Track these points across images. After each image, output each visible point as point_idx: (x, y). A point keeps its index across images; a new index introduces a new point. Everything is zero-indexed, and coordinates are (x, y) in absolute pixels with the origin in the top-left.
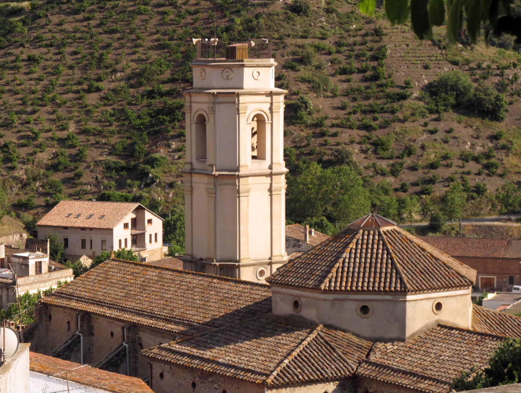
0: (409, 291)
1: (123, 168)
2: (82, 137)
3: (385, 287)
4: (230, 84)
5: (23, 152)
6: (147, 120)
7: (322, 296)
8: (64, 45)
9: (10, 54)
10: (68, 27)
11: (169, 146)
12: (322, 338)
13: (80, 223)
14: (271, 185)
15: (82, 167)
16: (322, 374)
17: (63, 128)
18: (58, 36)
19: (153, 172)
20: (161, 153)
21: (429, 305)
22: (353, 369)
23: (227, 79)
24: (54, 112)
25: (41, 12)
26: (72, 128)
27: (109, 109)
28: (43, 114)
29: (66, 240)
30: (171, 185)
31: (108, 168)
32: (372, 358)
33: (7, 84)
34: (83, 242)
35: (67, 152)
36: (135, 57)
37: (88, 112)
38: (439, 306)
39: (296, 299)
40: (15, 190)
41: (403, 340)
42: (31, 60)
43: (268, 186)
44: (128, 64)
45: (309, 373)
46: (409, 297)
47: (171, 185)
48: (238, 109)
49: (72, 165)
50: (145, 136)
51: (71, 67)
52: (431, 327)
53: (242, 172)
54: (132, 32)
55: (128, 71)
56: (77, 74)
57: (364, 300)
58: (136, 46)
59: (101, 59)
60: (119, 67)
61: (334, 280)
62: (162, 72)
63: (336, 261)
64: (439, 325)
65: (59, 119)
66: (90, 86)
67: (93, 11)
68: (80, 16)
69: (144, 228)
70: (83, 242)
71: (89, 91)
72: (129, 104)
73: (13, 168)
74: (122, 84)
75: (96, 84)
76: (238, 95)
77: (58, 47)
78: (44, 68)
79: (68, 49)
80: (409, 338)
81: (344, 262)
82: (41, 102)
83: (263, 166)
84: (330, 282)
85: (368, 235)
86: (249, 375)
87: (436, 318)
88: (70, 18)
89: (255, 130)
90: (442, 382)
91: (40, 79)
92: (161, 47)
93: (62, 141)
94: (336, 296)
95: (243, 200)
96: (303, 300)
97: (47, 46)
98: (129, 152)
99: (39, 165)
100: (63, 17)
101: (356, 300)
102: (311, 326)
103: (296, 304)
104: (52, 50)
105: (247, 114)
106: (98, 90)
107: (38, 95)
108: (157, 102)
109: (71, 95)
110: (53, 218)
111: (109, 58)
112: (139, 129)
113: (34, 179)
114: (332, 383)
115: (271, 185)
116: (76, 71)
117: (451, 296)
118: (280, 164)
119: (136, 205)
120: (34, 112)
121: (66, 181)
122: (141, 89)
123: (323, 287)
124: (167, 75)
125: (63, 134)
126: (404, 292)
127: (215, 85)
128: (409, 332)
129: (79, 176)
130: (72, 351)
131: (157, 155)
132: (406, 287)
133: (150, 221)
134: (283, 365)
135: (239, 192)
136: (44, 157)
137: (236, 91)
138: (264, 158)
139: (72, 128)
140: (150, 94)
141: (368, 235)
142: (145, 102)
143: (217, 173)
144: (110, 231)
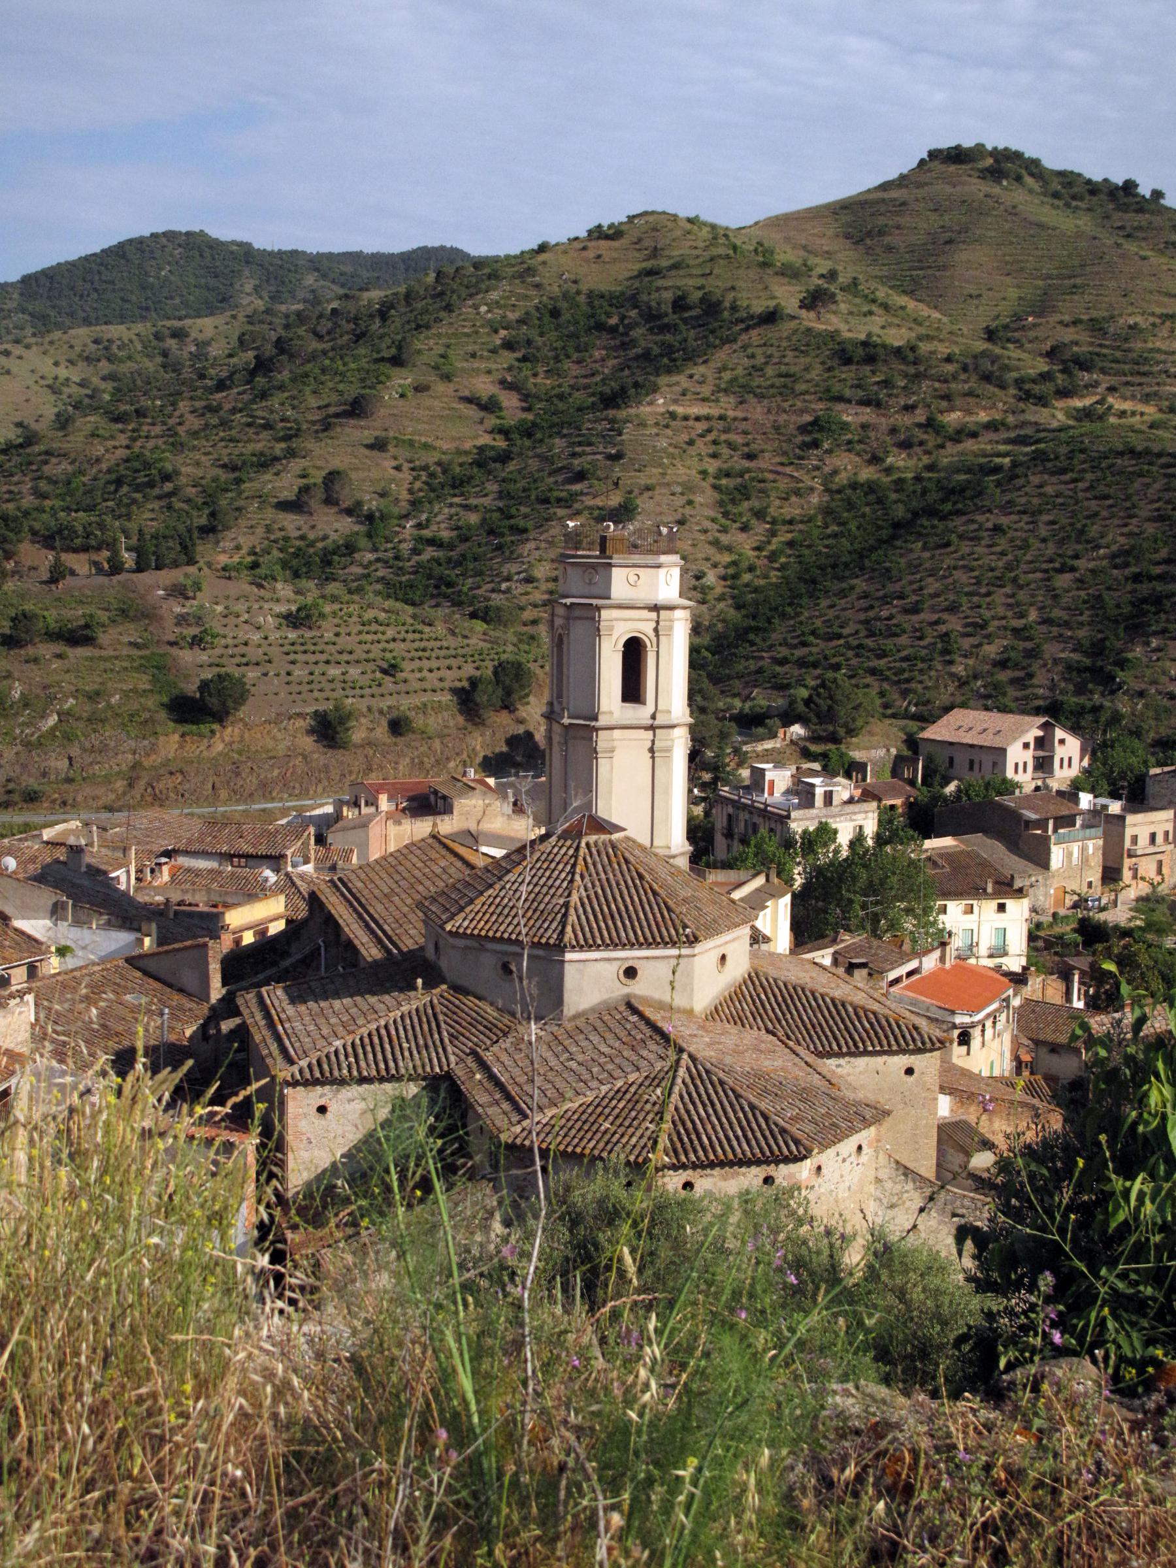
1: (1087, 669)
2: (1044, 628)
4: (595, 590)
5: (966, 643)
6: (1127, 610)
10: (1049, 490)
11: (1148, 644)
13: (968, 739)
15: (1035, 666)
17: (1022, 616)
18: (1035, 501)
19: (1120, 676)
20: (1138, 651)
24: (1013, 596)
26: (1033, 615)
27: (1082, 593)
28: (999, 597)
29: (951, 760)
30: (1141, 694)
31: (1069, 668)
33: (963, 558)
34: (972, 763)
35: (1022, 645)
36: (1126, 530)
37: (1055, 597)
38: (631, 973)
40: (951, 689)
42: (997, 529)
44: (1117, 539)
46: (569, 956)
47: (1141, 694)
49: (1025, 663)
50: (1121, 630)
51: (1044, 540)
53: (603, 721)
54: (1128, 498)
55: (1114, 548)
56: (1051, 549)
57: (505, 953)
58: (1130, 517)
59: (1082, 532)
60: (1103, 542)
62: (1156, 551)
65: (1018, 604)
66: (1063, 565)
67: (1084, 471)
68: (1067, 477)
69: (1052, 749)
70: (972, 763)
71: (1060, 571)
72: (1109, 589)
73: (951, 662)
74: (1105, 562)
75: (1070, 562)
76: (598, 609)
77: (1033, 514)
78: (1012, 540)
79: (1045, 518)
82: (999, 582)
83: (642, 713)
87: (626, 990)
88: (1054, 479)
91: (1003, 554)
92: (1161, 518)
93: (1016, 631)
94: (469, 942)
95: (603, 767)
98: (1097, 649)
99: (985, 660)
104: (1025, 518)
106: (1073, 569)
107: (997, 573)
108: (1144, 588)
109: (1039, 575)
110: (938, 732)
111: (1094, 530)
112: (1117, 622)
113: (975, 677)
116: (1050, 545)
119: (1043, 720)
120: (988, 594)
121: (1014, 681)
122: (1127, 572)
124: (1164, 553)
125: (1018, 623)
127: (574, 591)
129: (1031, 676)
130: (308, 966)
131: (1130, 655)
133: (1062, 742)
136: (991, 650)
137: (594, 602)
139: (1033, 615)
140: (1137, 578)
142: (1129, 587)
144: (1002, 751)
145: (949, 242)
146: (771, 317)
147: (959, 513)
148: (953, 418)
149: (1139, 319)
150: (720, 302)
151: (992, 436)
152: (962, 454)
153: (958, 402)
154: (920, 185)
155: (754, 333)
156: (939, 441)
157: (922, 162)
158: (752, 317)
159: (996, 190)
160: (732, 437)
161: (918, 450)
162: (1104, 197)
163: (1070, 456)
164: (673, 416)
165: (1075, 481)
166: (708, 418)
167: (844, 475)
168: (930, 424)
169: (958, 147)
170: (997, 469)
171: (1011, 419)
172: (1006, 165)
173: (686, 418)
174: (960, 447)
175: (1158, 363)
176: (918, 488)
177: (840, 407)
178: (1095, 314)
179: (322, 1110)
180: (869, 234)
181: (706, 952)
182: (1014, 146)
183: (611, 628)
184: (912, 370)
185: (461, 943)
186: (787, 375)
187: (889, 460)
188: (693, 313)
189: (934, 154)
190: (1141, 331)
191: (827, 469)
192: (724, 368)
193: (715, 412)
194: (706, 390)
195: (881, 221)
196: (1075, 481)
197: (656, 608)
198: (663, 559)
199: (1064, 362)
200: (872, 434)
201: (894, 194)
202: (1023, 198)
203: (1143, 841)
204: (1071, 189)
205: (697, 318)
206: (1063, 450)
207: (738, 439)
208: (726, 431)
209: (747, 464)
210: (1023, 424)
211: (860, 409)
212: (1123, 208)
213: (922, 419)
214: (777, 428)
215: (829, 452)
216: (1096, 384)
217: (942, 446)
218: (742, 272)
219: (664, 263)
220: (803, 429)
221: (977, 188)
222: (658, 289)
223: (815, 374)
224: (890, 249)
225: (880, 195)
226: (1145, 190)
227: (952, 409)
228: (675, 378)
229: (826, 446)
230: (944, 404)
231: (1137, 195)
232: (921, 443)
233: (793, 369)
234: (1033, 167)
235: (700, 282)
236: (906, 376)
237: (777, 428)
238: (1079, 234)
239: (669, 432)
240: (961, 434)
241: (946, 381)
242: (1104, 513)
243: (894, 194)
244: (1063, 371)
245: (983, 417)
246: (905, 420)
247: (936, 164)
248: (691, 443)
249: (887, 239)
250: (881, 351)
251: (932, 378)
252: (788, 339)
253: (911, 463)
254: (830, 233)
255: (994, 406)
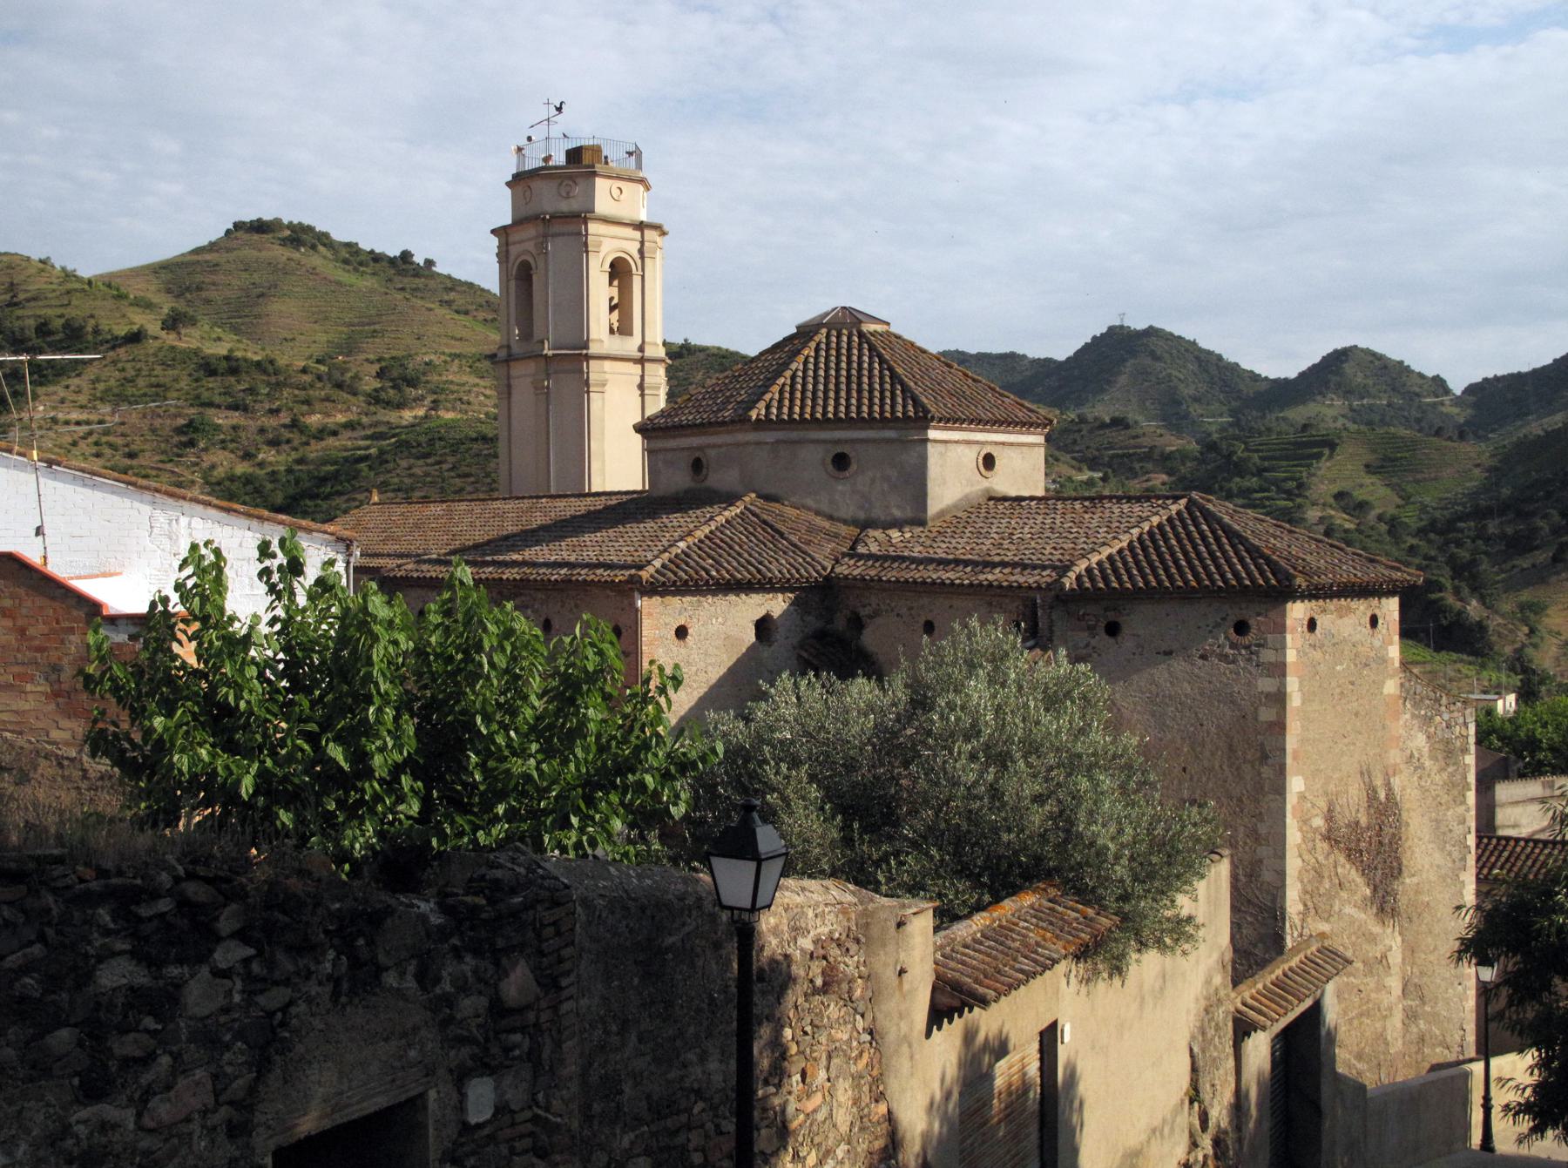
0: (933, 418)
3: (882, 412)
7: (752, 436)
8: (413, 489)
9: (354, 500)
12: (754, 514)
14: (642, 377)
16: (759, 571)
18: (407, 480)
21: (971, 456)
22: (824, 569)
23: (568, 197)
25: (389, 457)
32: (861, 549)
39: (697, 454)
41: (922, 523)
43: (638, 380)
45: (732, 568)
46: (933, 434)
48: (586, 244)
52: (975, 503)
53: (594, 349)
54: (488, 475)
57: (838, 442)
61: (775, 404)
63: (779, 374)
64: (990, 499)
80: (933, 519)
81: (793, 377)
83: (630, 346)
84: (768, 407)
85: (839, 337)
86: (599, 572)
87: (985, 484)
88: (421, 462)
89: (615, 301)
90: (1034, 567)
94: (780, 435)
96: (712, 453)
97: (394, 490)
100: (412, 461)
101: (824, 442)
102: (730, 499)
103: (697, 466)
104: (400, 495)
105: (602, 255)
114: (780, 596)
115: (642, 377)
117: (1012, 444)
118: (656, 344)
123: (753, 415)
126: (923, 419)
128: (933, 507)
132: (926, 411)
134: (674, 551)
135: (587, 383)
138: (631, 334)
141: (839, 337)
143: (550, 353)
145: (262, 295)
146: (136, 338)
147: (339, 493)
148: (314, 420)
149: (433, 357)
150: (82, 328)
151: (349, 434)
152: (324, 449)
153: (318, 406)
154: (228, 250)
155: (121, 351)
156: (304, 439)
157: (228, 232)
158: (117, 338)
159: (296, 255)
160: (111, 439)
161: (286, 447)
162: (385, 264)
163: (431, 442)
164: (54, 420)
165: (439, 463)
166: (88, 423)
167: (220, 469)
168: (294, 424)
169: (259, 220)
170: (366, 458)
171: (365, 420)
172: (301, 236)
173: (67, 423)
174: (323, 444)
175: (453, 392)
176: (291, 478)
177: (211, 411)
178: (394, 353)
179: (681, 632)
180: (188, 289)
182: (306, 222)
183: (599, 244)
184: (273, 379)
185: (769, 436)
186: (158, 386)
187: (261, 456)
188: (57, 337)
189: (238, 226)
190: (435, 367)
191: (204, 465)
192: (97, 380)
193: (94, 417)
194: (83, 399)
195: (198, 278)
196: (439, 463)
197: (640, 226)
199: (392, 380)
200: (243, 434)
201: (208, 257)
202: (318, 260)
204: (352, 256)
205: (61, 341)
206: (423, 439)
207: (119, 441)
208: (106, 433)
209: (128, 462)
210: (376, 424)
211: (230, 413)
212: (402, 274)
213: (287, 421)
214: (153, 431)
215: (206, 450)
216: (422, 398)
217: (307, 444)
218: (99, 303)
219: (22, 296)
220: (179, 431)
221: (281, 253)
222: (18, 318)
223: (184, 384)
224: (208, 301)
225: (195, 258)
226: (419, 259)
227: (313, 413)
228: (51, 389)
229: (202, 445)
230: (305, 408)
231: (412, 263)
232: (288, 441)
233: (162, 380)
234: (324, 239)
235: (59, 311)
236: (269, 384)
237: (153, 431)
238: (372, 291)
239: (51, 434)
240: (322, 433)
241: (304, 389)
242: (469, 488)
243: (208, 257)
244: (393, 387)
245: (341, 418)
246: (271, 422)
247: (239, 234)
248: (75, 444)
249: (204, 294)
250: (243, 364)
251: (291, 386)
252: (155, 355)
253: (281, 458)
254: (153, 288)
255: (349, 409)
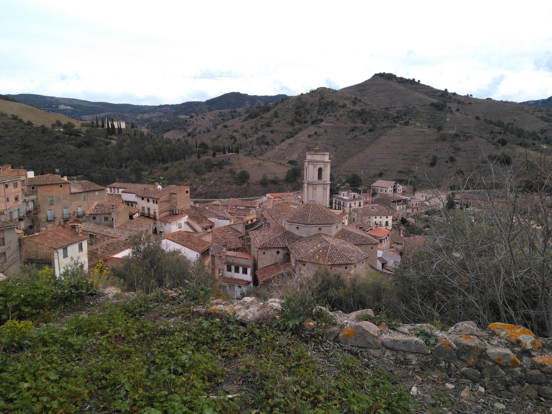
38: (320, 229)
172: (390, 77)
179: (264, 253)
181: (334, 227)
189: (376, 75)
198: (326, 153)
202: (393, 83)
203: (414, 205)
226: (417, 80)
234: (394, 76)
